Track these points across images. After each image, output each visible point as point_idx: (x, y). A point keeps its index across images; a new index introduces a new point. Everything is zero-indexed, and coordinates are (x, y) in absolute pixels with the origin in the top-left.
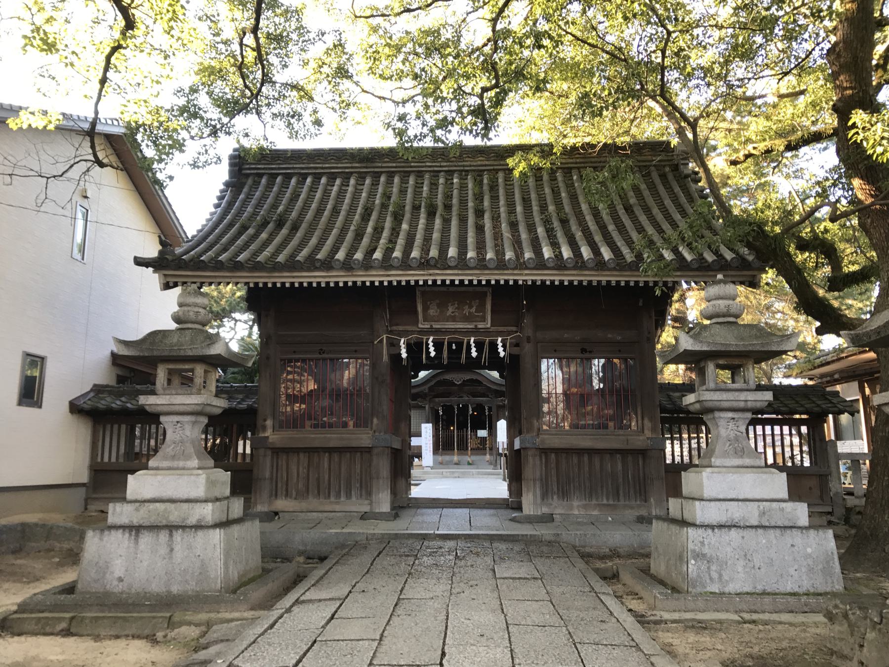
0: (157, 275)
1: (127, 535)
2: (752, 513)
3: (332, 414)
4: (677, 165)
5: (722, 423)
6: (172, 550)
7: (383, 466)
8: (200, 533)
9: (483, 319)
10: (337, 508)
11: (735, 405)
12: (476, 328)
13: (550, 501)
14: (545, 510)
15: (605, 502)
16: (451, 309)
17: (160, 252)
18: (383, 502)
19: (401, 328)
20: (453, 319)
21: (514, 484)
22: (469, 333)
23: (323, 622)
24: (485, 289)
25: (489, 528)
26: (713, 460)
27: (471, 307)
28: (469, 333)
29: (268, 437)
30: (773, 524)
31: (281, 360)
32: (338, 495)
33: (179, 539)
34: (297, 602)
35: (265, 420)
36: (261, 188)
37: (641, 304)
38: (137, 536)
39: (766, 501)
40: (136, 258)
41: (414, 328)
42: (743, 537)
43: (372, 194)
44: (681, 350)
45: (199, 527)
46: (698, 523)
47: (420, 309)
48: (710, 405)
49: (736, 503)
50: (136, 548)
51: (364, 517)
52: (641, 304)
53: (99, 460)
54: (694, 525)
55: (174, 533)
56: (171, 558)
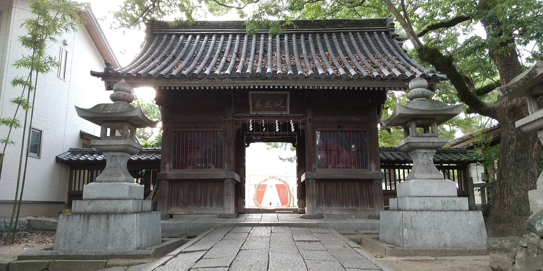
0: (104, 82)
1: (82, 218)
2: (438, 203)
3: (202, 162)
4: (388, 31)
5: (420, 155)
6: (108, 226)
7: (230, 190)
8: (125, 217)
9: (285, 110)
10: (205, 212)
11: (427, 145)
12: (281, 114)
13: (321, 207)
14: (318, 212)
15: (351, 207)
16: (268, 104)
17: (105, 69)
18: (230, 208)
19: (240, 115)
20: (269, 109)
21: (301, 201)
22: (277, 117)
23: (196, 260)
24: (286, 92)
25: (288, 221)
26: (415, 175)
27: (279, 103)
28: (277, 117)
29: (166, 174)
30: (449, 209)
31: (175, 132)
32: (205, 204)
33: (113, 220)
34: (181, 252)
35: (165, 164)
36: (163, 41)
37: (370, 102)
38: (88, 219)
39: (446, 197)
40: (91, 72)
41: (248, 115)
42: (434, 216)
43: (224, 44)
44: (397, 115)
45: (124, 213)
46: (408, 209)
47: (251, 104)
48: (413, 145)
49: (429, 198)
50: (88, 223)
51: (220, 216)
52: (370, 102)
53: (73, 189)
54: (405, 210)
55: (110, 216)
56: (108, 231)
